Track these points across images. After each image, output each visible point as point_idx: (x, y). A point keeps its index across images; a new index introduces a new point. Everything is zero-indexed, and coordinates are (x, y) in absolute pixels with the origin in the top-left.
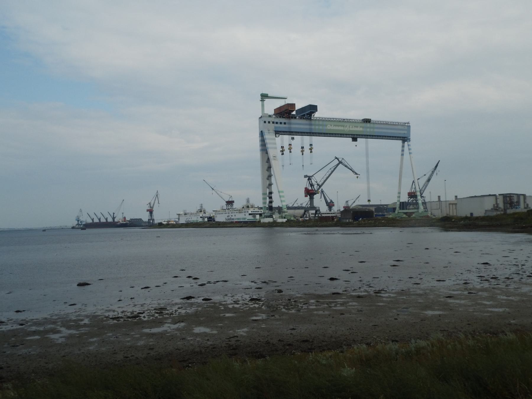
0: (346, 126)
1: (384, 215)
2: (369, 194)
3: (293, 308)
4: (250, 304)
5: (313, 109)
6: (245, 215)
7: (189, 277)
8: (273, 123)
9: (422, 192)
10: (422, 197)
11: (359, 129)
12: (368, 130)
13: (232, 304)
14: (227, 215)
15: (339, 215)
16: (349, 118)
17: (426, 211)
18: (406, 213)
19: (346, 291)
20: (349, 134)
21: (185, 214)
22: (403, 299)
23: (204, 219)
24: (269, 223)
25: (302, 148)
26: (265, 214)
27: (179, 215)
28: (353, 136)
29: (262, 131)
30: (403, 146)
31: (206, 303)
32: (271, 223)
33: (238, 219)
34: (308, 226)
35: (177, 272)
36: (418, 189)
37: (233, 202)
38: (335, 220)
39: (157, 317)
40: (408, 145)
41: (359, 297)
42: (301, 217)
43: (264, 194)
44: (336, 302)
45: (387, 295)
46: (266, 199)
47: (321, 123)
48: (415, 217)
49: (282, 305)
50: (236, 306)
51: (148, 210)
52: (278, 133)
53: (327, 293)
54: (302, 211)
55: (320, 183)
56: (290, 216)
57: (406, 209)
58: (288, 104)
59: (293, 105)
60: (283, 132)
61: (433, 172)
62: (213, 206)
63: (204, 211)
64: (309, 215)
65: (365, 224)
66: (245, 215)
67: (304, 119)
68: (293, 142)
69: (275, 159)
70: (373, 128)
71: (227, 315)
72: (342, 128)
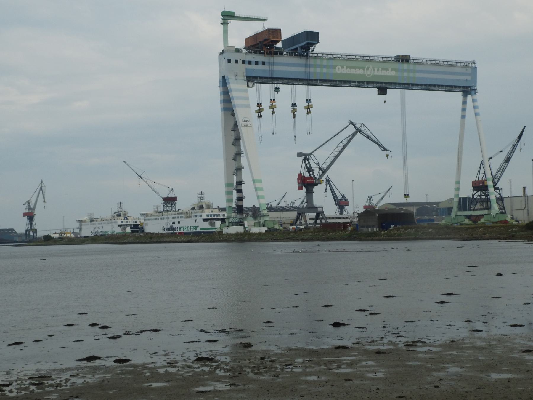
0: (368, 69)
1: (433, 220)
2: (406, 184)
3: (266, 372)
4: (195, 366)
5: (310, 38)
6: (196, 221)
7: (94, 325)
8: (244, 62)
9: (496, 180)
10: (495, 189)
11: (390, 73)
12: (405, 74)
13: (164, 367)
14: (166, 221)
15: (356, 221)
16: (372, 53)
17: (502, 213)
18: (469, 217)
19: (358, 343)
20: (373, 83)
21: (92, 220)
22: (450, 355)
23: (125, 229)
24: (237, 234)
25: (294, 105)
26: (231, 220)
27: (80, 221)
28: (379, 86)
29: (224, 77)
30: (464, 103)
31: (121, 367)
32: (241, 234)
33: (185, 228)
34: (303, 240)
35: (73, 318)
36: (489, 176)
37: (175, 199)
38: (349, 228)
39: (33, 391)
40: (474, 101)
41: (379, 352)
42: (292, 225)
43: (229, 185)
44: (339, 361)
45: (425, 349)
46: (232, 193)
47: (325, 62)
48: (484, 223)
49: (249, 367)
50: (171, 370)
51: (25, 215)
52: (251, 79)
53: (325, 347)
54: (293, 215)
55: (324, 167)
56: (274, 222)
57: (470, 210)
58: (269, 30)
59: (277, 32)
60: (261, 78)
61: (515, 146)
62: (142, 206)
63: (125, 214)
64: (306, 221)
65: (399, 235)
66: (196, 221)
67: (295, 55)
68: (277, 96)
69: (246, 126)
70: (414, 71)
71: (155, 385)
72: (361, 72)
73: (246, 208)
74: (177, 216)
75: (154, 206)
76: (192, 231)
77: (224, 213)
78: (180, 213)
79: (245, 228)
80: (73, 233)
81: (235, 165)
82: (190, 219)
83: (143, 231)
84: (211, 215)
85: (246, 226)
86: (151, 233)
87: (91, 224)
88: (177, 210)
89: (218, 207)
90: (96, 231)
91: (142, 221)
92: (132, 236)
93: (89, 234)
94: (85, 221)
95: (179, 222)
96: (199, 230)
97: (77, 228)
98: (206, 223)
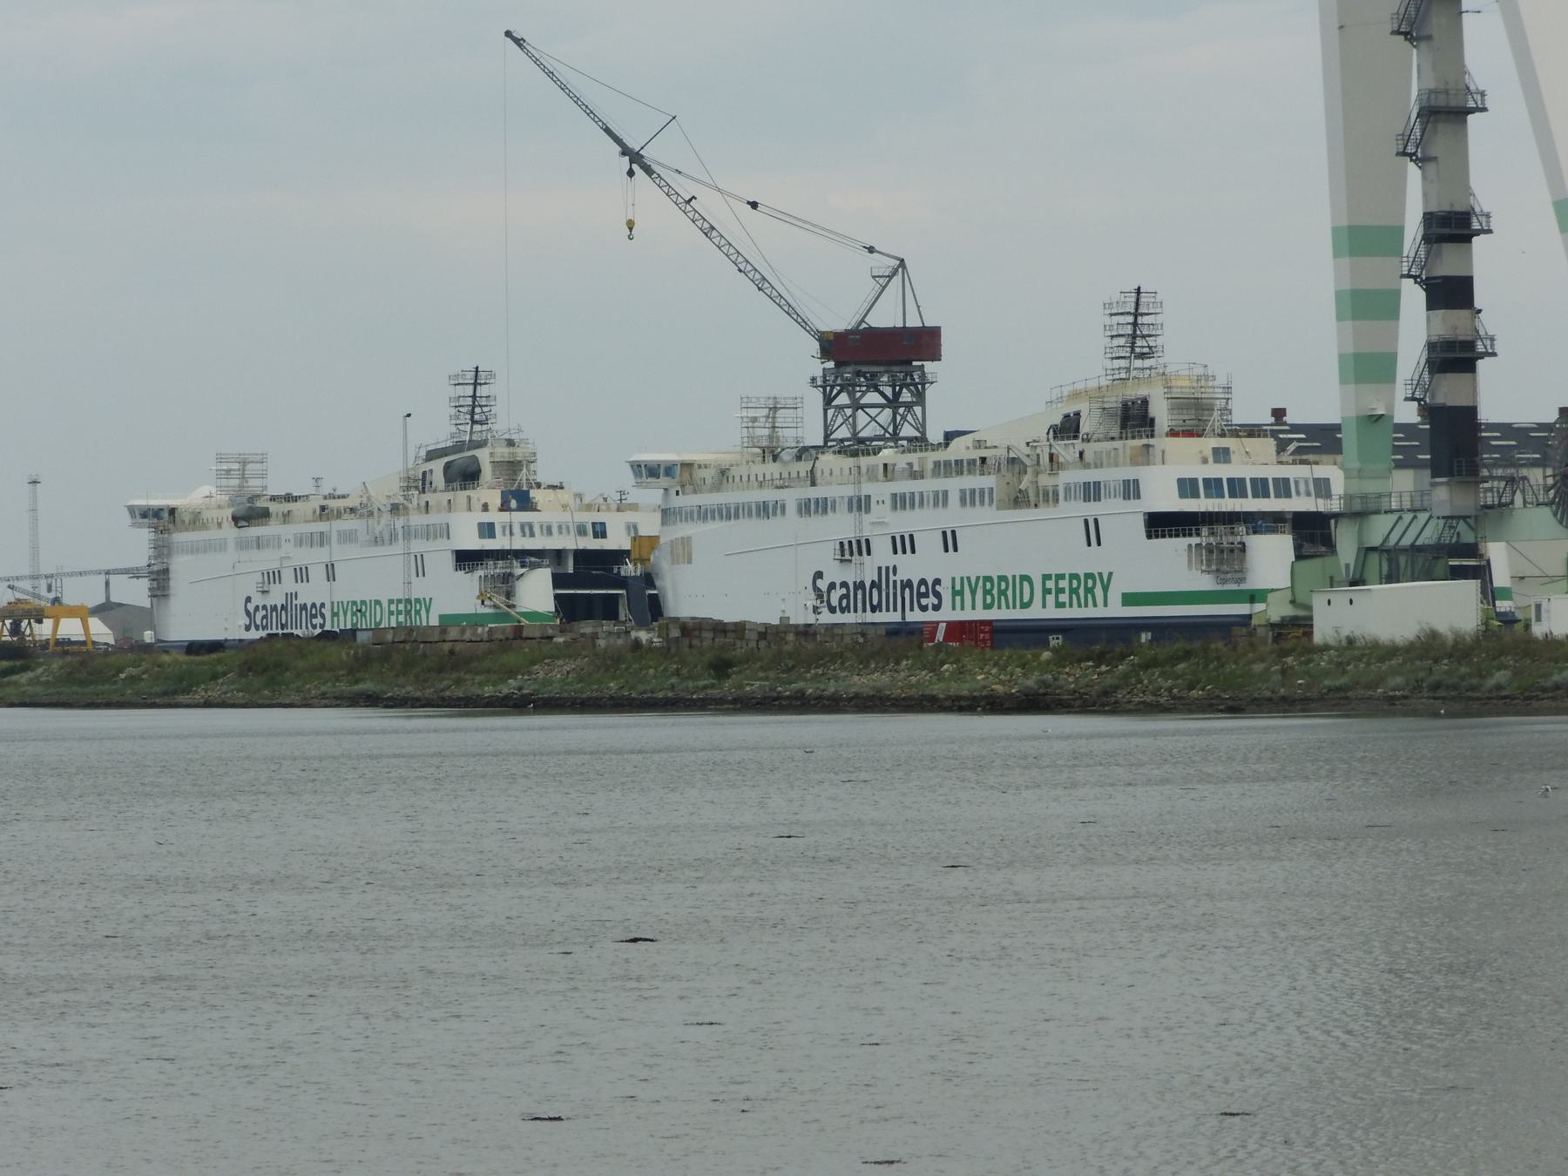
6: (1093, 533)
14: (842, 526)
23: (506, 584)
24: (1429, 647)
26: (1379, 529)
27: (162, 520)
32: (1460, 650)
37: (925, 342)
43: (1361, 240)
62: (650, 404)
63: (512, 467)
66: (1093, 533)
73: (1506, 429)
74: (929, 485)
76: (1052, 613)
77: (1321, 471)
78: (958, 467)
79: (1490, 594)
80: (105, 610)
81: (1414, 78)
83: (655, 607)
84: (1214, 487)
85: (1501, 578)
86: (719, 628)
87: (242, 545)
88: (935, 436)
89: (1279, 414)
90: (276, 597)
91: (650, 525)
92: (568, 651)
93: (229, 626)
94: (196, 521)
95: (950, 541)
96: (1116, 609)
97: (134, 573)
98: (1176, 547)
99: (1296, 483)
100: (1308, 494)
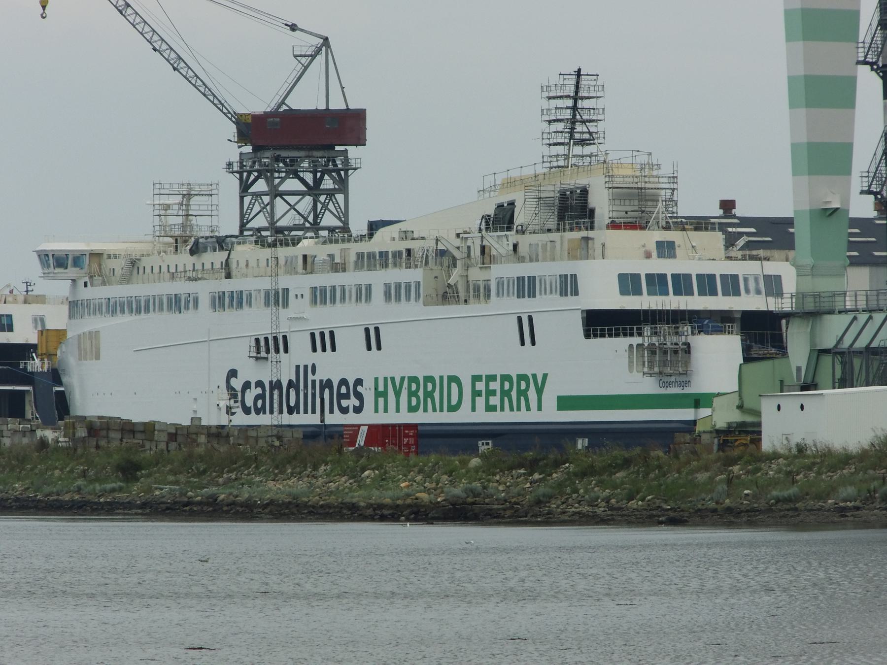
6: (527, 331)
14: (258, 321)
26: (833, 330)
33: (422, 389)
37: (347, 126)
46: (842, 94)
66: (527, 331)
74: (351, 278)
75: (159, 189)
76: (481, 416)
77: (773, 268)
78: (383, 260)
82: (475, 308)
83: (62, 403)
84: (657, 283)
86: (128, 428)
89: (727, 206)
91: (57, 318)
95: (373, 339)
98: (616, 348)
99: (746, 280)
100: (758, 292)
